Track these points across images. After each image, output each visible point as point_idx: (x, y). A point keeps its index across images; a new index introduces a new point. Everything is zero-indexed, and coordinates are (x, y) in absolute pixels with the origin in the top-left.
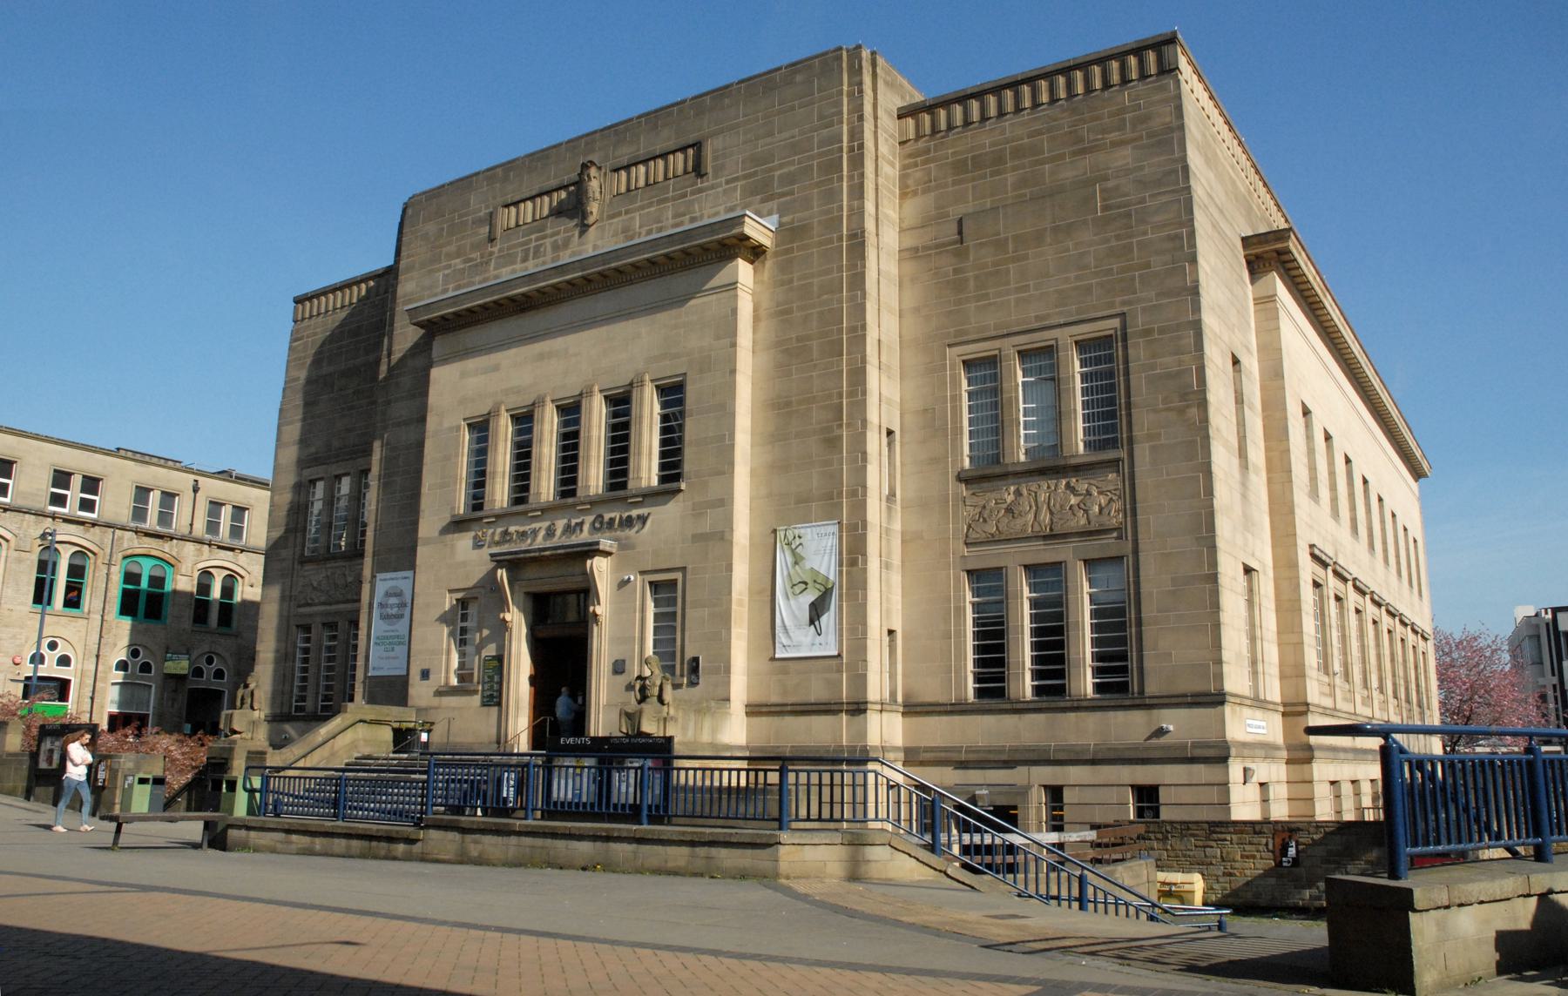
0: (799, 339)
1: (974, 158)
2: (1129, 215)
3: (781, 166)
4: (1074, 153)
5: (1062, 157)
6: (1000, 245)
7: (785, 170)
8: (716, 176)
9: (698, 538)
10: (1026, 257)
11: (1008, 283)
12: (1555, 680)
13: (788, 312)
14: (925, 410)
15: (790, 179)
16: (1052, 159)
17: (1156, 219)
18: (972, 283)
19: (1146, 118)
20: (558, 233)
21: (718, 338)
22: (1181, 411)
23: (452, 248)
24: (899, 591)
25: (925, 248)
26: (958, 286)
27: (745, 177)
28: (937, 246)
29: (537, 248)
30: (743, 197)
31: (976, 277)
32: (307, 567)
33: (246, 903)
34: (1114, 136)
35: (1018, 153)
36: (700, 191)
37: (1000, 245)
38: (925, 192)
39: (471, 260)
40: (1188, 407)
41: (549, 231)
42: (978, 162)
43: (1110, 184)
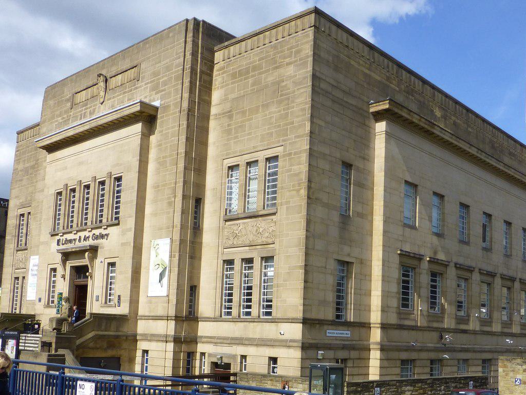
1: (239, 71)
2: (288, 99)
3: (163, 77)
5: (268, 70)
6: (244, 113)
7: (164, 79)
8: (142, 82)
10: (251, 119)
15: (165, 83)
16: (266, 72)
19: (298, 52)
21: (133, 157)
22: (298, 191)
23: (58, 113)
24: (381, 248)
25: (219, 114)
26: (228, 132)
27: (151, 82)
29: (85, 113)
30: (150, 92)
33: (249, 391)
34: (287, 60)
35: (255, 68)
36: (136, 88)
37: (244, 113)
38: (222, 87)
39: (63, 118)
42: (240, 73)
43: (284, 84)
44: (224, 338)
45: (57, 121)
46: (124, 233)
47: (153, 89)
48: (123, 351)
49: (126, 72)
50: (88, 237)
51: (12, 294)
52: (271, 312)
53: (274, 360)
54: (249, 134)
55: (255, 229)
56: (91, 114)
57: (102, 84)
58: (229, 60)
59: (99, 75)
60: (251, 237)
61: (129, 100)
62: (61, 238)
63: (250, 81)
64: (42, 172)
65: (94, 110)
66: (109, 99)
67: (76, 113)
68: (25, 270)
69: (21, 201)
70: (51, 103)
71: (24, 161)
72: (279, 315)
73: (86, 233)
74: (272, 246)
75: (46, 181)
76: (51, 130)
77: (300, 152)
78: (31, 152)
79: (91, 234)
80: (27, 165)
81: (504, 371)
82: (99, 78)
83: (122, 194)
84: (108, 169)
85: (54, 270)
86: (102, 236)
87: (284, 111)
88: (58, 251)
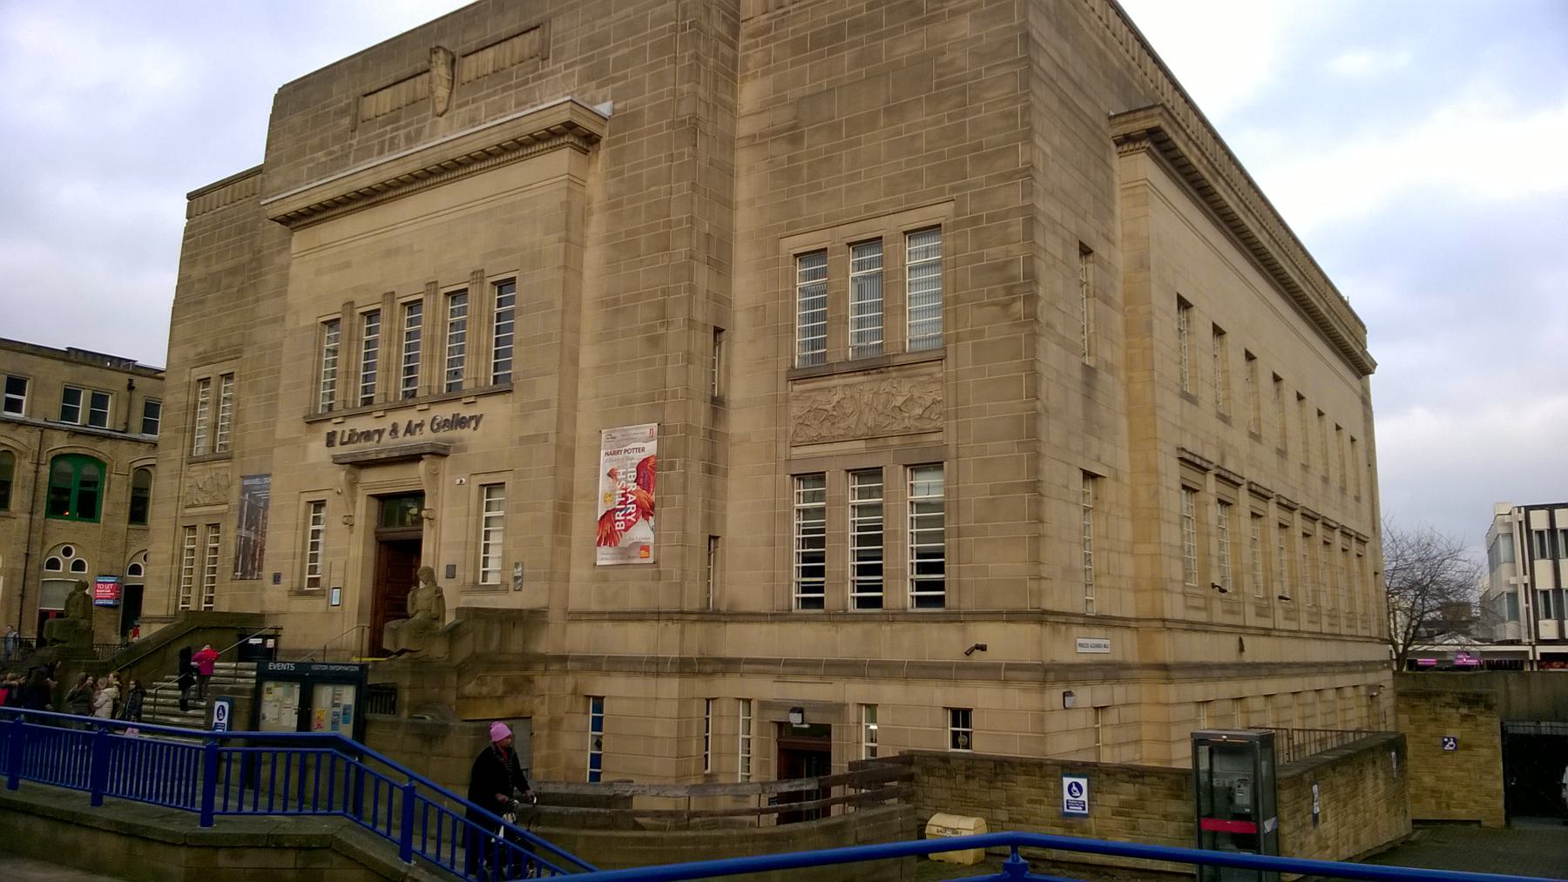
0: (628, 233)
2: (963, 92)
3: (616, 48)
4: (912, 26)
7: (619, 53)
8: (555, 62)
9: (524, 440)
10: (858, 143)
11: (839, 171)
12: (1527, 579)
13: (618, 205)
14: (756, 308)
17: (991, 94)
18: (805, 172)
20: (410, 124)
22: (1006, 306)
23: (316, 141)
25: (762, 136)
27: (583, 61)
28: (773, 134)
30: (581, 83)
31: (810, 166)
32: (195, 468)
35: (856, 26)
36: (540, 77)
38: (765, 73)
39: (332, 153)
40: (1014, 300)
41: (402, 123)
42: (818, 41)
43: (946, 58)
44: (816, 664)
45: (313, 160)
46: (526, 413)
47: (587, 77)
48: (537, 701)
49: (508, 43)
50: (420, 425)
51: (176, 566)
52: (942, 597)
53: (961, 716)
54: (852, 177)
55: (883, 398)
56: (410, 140)
57: (441, 70)
58: (780, 11)
59: (434, 51)
60: (869, 419)
61: (519, 104)
62: (339, 429)
63: (847, 56)
64: (272, 278)
65: (419, 133)
66: (459, 106)
67: (367, 140)
68: (225, 507)
69: (201, 349)
70: (297, 119)
71: (208, 259)
72: (968, 604)
73: (413, 416)
74: (934, 437)
75: (290, 297)
76: (296, 183)
77: (1007, 214)
78: (228, 236)
79: (427, 418)
80: (215, 267)
81: (1411, 721)
82: (434, 58)
83: (518, 322)
84: (477, 264)
85: (319, 505)
86: (460, 422)
87: (950, 119)
88: (337, 460)
